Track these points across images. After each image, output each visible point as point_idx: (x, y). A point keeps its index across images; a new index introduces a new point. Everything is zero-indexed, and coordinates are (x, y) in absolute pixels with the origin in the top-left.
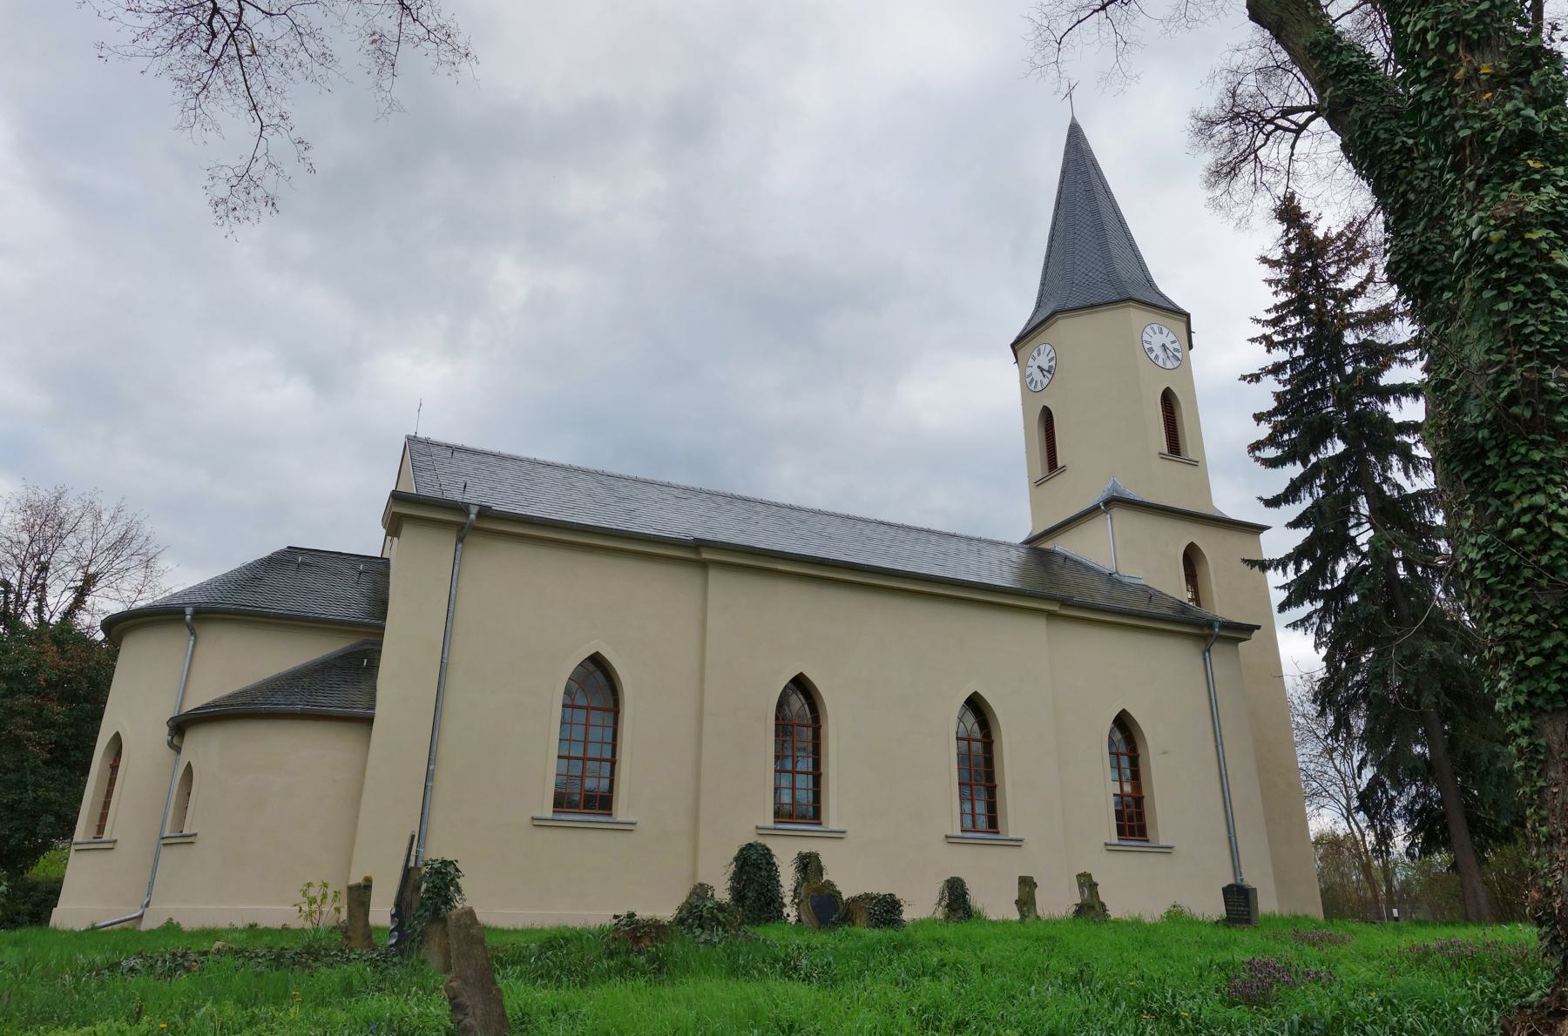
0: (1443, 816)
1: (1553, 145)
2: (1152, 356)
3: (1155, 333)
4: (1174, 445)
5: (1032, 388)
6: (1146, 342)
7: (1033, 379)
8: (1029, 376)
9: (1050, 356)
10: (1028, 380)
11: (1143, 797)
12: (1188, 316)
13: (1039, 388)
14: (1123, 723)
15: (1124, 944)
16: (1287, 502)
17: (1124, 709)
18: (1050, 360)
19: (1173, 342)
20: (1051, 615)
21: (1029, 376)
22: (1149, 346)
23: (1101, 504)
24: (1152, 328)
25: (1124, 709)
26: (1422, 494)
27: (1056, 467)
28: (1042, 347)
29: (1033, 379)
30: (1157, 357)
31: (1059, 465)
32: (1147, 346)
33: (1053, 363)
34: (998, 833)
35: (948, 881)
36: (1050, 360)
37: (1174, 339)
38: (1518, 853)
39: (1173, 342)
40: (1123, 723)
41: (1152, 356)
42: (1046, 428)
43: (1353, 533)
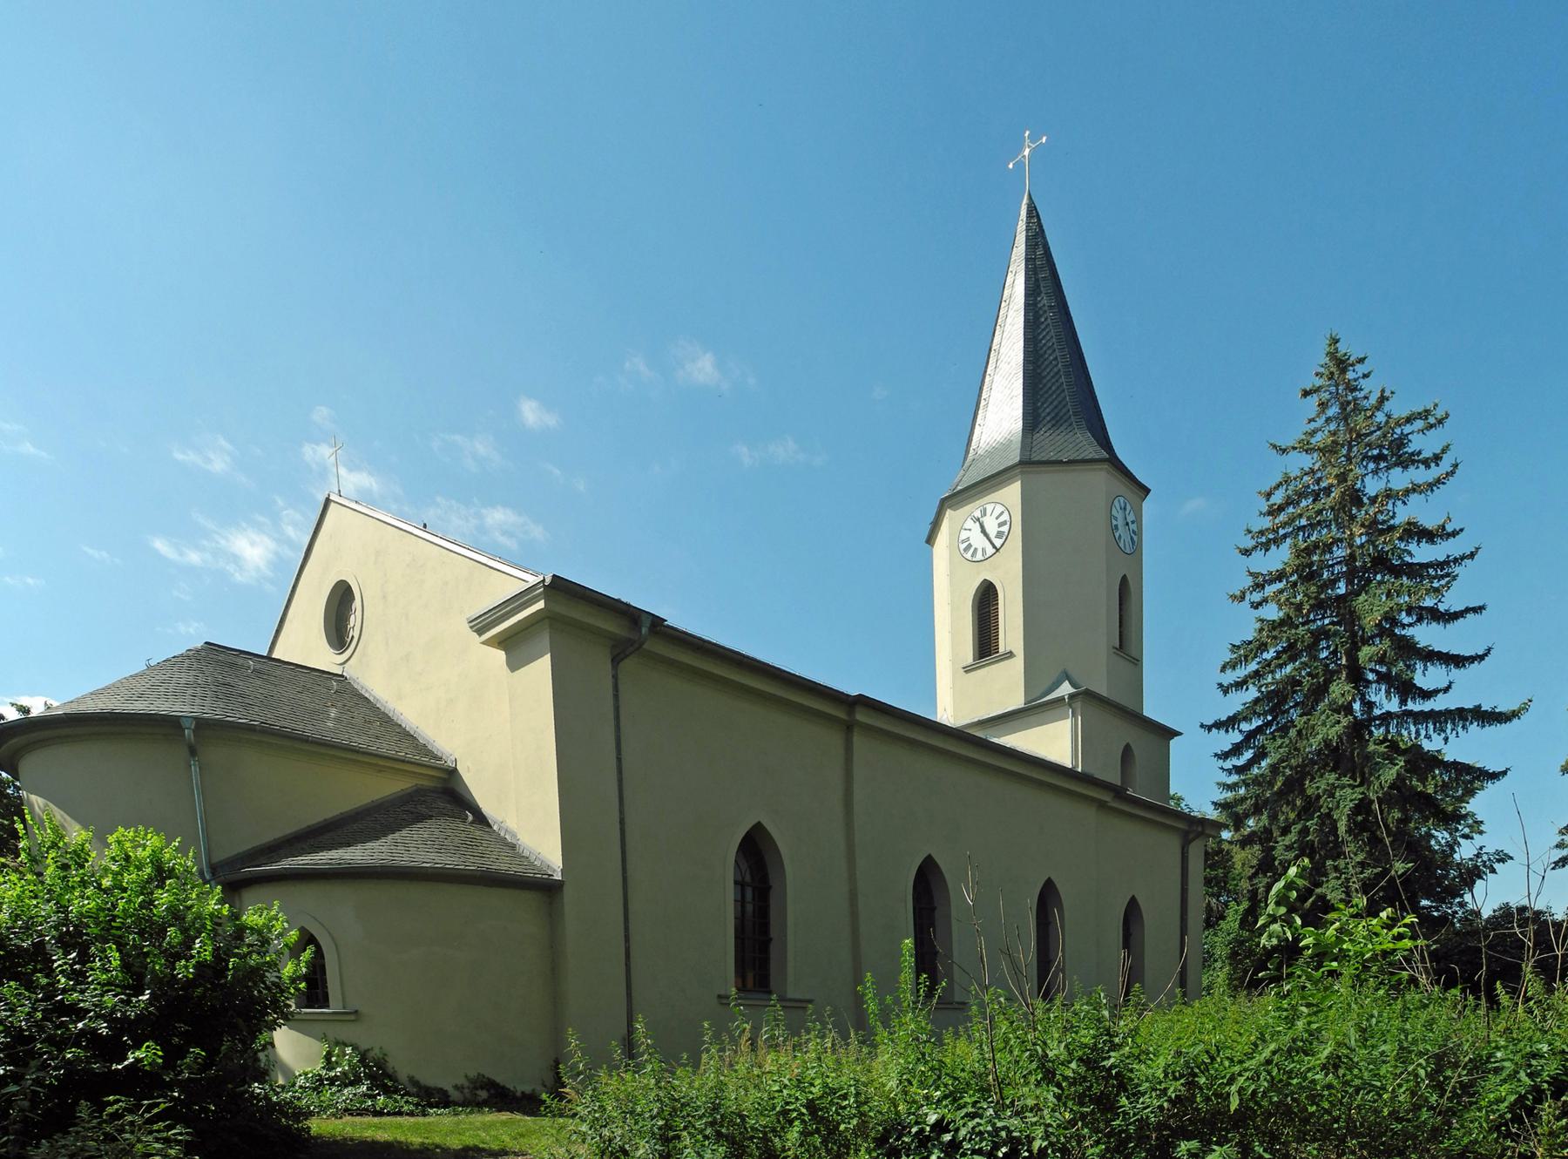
3: (997, 518)
7: (970, 546)
8: (963, 542)
9: (1002, 519)
10: (963, 546)
13: (979, 556)
14: (1133, 906)
15: (1274, 1074)
16: (1487, 772)
17: (759, 822)
18: (1001, 525)
20: (1102, 805)
21: (963, 542)
23: (1066, 697)
25: (759, 822)
26: (286, 509)
28: (989, 508)
31: (1001, 650)
33: (1005, 529)
38: (940, 1127)
40: (1133, 906)
42: (981, 599)
43: (1269, 774)
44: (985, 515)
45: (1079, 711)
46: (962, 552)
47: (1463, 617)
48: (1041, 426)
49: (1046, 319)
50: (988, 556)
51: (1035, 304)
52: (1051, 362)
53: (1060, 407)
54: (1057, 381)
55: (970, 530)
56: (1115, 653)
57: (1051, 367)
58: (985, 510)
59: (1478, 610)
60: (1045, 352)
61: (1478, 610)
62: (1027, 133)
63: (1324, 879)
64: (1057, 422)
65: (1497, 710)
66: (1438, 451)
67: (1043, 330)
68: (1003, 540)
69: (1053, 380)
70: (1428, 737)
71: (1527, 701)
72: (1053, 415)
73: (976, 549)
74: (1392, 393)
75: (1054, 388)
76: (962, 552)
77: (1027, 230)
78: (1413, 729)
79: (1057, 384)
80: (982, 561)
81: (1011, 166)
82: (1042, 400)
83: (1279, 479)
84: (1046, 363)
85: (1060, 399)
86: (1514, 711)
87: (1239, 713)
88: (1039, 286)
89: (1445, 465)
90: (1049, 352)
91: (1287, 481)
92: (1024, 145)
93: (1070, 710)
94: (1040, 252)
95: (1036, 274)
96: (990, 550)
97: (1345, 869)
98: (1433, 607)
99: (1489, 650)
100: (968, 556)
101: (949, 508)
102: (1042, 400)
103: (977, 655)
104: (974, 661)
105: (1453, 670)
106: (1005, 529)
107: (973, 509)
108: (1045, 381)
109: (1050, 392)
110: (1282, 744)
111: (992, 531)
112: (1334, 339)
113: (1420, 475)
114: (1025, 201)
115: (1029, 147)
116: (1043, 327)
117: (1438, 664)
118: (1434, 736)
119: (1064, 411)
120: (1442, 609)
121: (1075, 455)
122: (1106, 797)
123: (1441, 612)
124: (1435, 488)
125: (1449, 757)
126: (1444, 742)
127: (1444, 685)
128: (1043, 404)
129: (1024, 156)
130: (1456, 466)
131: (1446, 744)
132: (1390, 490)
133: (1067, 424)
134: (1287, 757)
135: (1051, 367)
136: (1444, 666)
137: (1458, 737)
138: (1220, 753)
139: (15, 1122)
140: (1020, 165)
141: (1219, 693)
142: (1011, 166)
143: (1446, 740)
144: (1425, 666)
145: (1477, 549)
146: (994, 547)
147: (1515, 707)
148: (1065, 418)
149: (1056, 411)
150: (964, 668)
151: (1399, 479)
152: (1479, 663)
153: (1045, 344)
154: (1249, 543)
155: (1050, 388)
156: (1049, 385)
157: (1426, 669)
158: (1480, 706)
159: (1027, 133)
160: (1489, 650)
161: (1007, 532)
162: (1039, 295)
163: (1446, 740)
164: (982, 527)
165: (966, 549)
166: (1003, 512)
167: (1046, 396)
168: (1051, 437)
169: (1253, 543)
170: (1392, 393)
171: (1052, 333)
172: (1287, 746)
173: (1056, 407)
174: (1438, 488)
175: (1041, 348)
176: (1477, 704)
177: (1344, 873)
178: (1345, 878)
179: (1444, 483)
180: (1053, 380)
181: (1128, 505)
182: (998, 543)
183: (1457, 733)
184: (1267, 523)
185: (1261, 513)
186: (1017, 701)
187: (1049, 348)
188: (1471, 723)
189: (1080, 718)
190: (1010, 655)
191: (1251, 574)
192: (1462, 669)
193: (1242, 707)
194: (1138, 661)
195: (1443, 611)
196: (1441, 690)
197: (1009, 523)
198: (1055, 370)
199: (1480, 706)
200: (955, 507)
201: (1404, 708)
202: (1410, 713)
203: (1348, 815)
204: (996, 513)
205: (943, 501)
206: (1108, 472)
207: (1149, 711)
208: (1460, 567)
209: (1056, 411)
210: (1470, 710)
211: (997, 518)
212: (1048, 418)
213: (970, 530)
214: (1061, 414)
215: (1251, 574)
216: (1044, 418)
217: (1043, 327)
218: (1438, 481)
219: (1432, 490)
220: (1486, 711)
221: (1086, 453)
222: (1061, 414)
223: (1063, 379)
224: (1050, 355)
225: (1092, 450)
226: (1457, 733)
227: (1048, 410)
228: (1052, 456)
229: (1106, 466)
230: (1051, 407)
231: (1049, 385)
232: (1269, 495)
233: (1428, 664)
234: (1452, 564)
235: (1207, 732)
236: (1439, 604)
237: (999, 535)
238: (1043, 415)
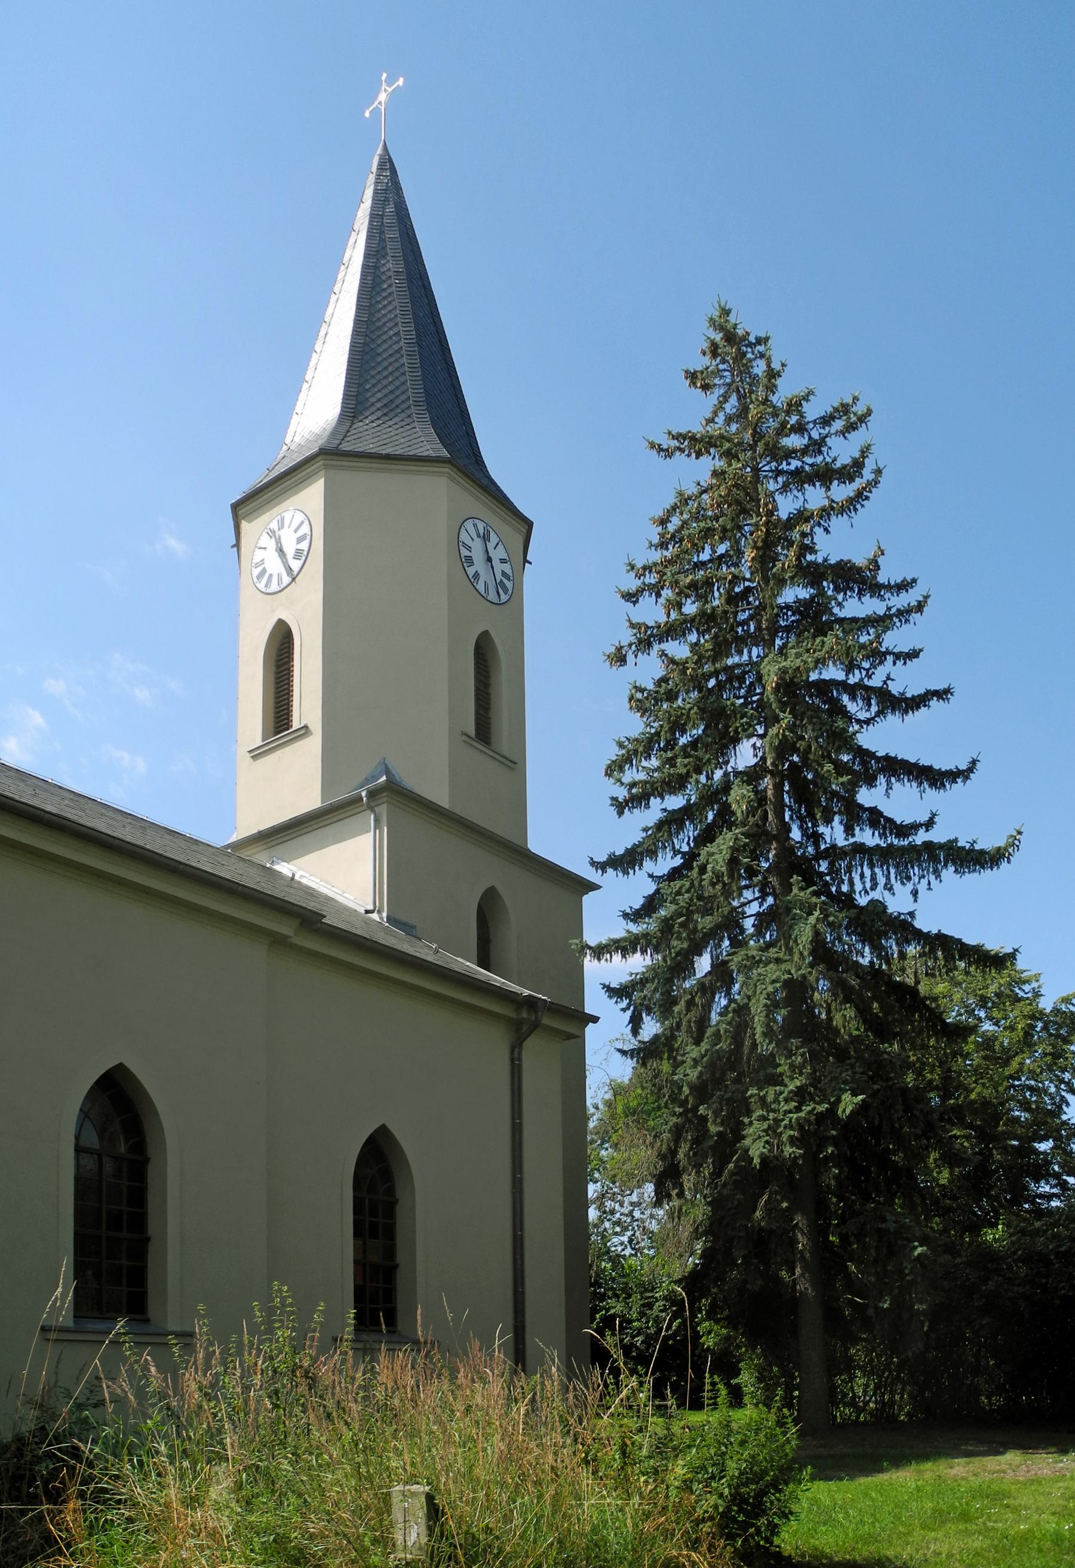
0: (885, 889)
1: (615, 1491)
2: (471, 571)
3: (296, 531)
4: (484, 732)
5: (262, 586)
6: (465, 545)
7: (264, 571)
8: (257, 565)
9: (300, 533)
11: (397, 1265)
12: (529, 525)
13: (274, 587)
18: (300, 540)
19: (503, 561)
20: (278, 942)
21: (257, 565)
22: (467, 553)
24: (475, 525)
27: (288, 726)
28: (288, 516)
29: (264, 571)
30: (476, 575)
31: (296, 725)
32: (464, 552)
34: (147, 1321)
35: (626, 873)
36: (300, 540)
37: (505, 556)
39: (503, 561)
41: (471, 571)
44: (283, 527)
45: (384, 820)
46: (255, 580)
47: (925, 706)
48: (367, 413)
49: (390, 286)
50: (284, 585)
51: (376, 268)
52: (391, 338)
53: (399, 392)
54: (396, 360)
55: (265, 548)
56: (464, 741)
57: (390, 342)
58: (283, 519)
59: (942, 694)
60: (384, 324)
61: (942, 694)
62: (385, 75)
63: (746, 1120)
64: (390, 410)
65: (977, 847)
66: (857, 455)
67: (385, 298)
68: (302, 562)
69: (392, 360)
70: (889, 887)
71: (1015, 833)
72: (385, 401)
73: (271, 576)
74: (783, 365)
75: (390, 369)
76: (255, 580)
77: (376, 183)
78: (867, 872)
79: (397, 365)
80: (280, 591)
81: (367, 114)
82: (374, 381)
83: (671, 500)
84: (385, 337)
85: (397, 383)
86: (999, 849)
87: (635, 847)
88: (384, 248)
89: (867, 474)
90: (389, 325)
91: (684, 500)
92: (380, 89)
93: (372, 816)
94: (390, 209)
95: (382, 232)
96: (286, 579)
97: (774, 1102)
98: (882, 688)
99: (974, 762)
100: (262, 586)
101: (243, 518)
102: (374, 381)
103: (272, 729)
104: (263, 741)
105: (928, 790)
106: (304, 545)
107: (268, 519)
108: (379, 359)
109: (386, 373)
110: (681, 887)
111: (290, 550)
112: (723, 309)
113: (841, 492)
114: (379, 151)
115: (385, 90)
116: (384, 294)
117: (906, 780)
118: (897, 886)
119: (403, 397)
120: (894, 692)
121: (403, 451)
122: (285, 928)
123: (894, 696)
124: (858, 506)
125: (924, 923)
126: (911, 899)
127: (924, 818)
128: (374, 386)
129: (380, 103)
130: (878, 472)
131: (916, 901)
132: (805, 509)
133: (404, 415)
134: (688, 909)
135: (390, 342)
136: (914, 784)
137: (930, 889)
138: (628, 911)
139: (154, 1405)
140: (376, 112)
141: (613, 812)
142: (367, 114)
143: (915, 893)
144: (889, 782)
145: (926, 597)
146: (289, 570)
147: (1001, 843)
148: (404, 406)
149: (391, 397)
150: (250, 752)
151: (815, 497)
152: (964, 782)
153: (384, 315)
154: (632, 583)
155: (385, 368)
156: (385, 364)
157: (889, 787)
158: (956, 840)
159: (385, 75)
160: (974, 762)
161: (306, 549)
162: (384, 257)
163: (915, 893)
164: (278, 541)
165: (260, 576)
166: (302, 523)
167: (378, 377)
168: (378, 429)
169: (639, 583)
170: (783, 365)
171: (396, 303)
172: (688, 891)
173: (392, 392)
174: (863, 506)
175: (379, 319)
176: (952, 837)
177: (774, 1111)
178: (775, 1120)
179: (867, 498)
180: (392, 360)
181: (492, 534)
182: (296, 565)
183: (929, 883)
184: (656, 556)
185: (651, 545)
186: (311, 800)
187: (390, 320)
188: (946, 866)
189: (385, 829)
190: (305, 731)
191: (632, 625)
192: (942, 791)
193: (644, 835)
194: (515, 763)
195: (897, 694)
196: (921, 825)
197: (309, 538)
198: (396, 347)
199: (956, 840)
200: (251, 515)
201: (852, 840)
202: (860, 849)
203: (766, 1005)
204: (295, 525)
205: (236, 507)
206: (453, 479)
207: (538, 843)
208: (907, 625)
209: (391, 397)
210: (941, 846)
211: (296, 531)
212: (379, 405)
213: (265, 548)
214: (397, 402)
215: (632, 625)
216: (373, 404)
217: (384, 294)
218: (860, 496)
219: (856, 510)
220: (963, 848)
221: (421, 450)
222: (397, 402)
223: (404, 360)
224: (391, 329)
225: (428, 444)
226: (929, 883)
227: (379, 395)
228: (370, 447)
229: (447, 470)
230: (385, 391)
231: (385, 364)
232: (663, 522)
233: (893, 779)
234: (895, 620)
235: (600, 871)
236: (889, 682)
237: (298, 554)
238: (372, 400)
